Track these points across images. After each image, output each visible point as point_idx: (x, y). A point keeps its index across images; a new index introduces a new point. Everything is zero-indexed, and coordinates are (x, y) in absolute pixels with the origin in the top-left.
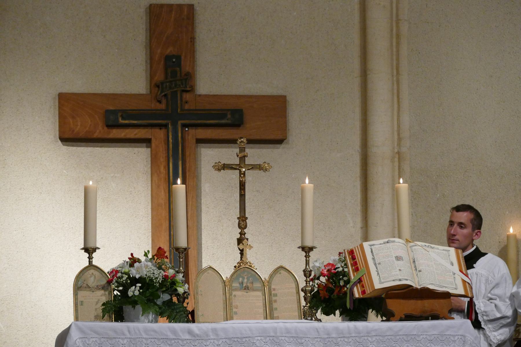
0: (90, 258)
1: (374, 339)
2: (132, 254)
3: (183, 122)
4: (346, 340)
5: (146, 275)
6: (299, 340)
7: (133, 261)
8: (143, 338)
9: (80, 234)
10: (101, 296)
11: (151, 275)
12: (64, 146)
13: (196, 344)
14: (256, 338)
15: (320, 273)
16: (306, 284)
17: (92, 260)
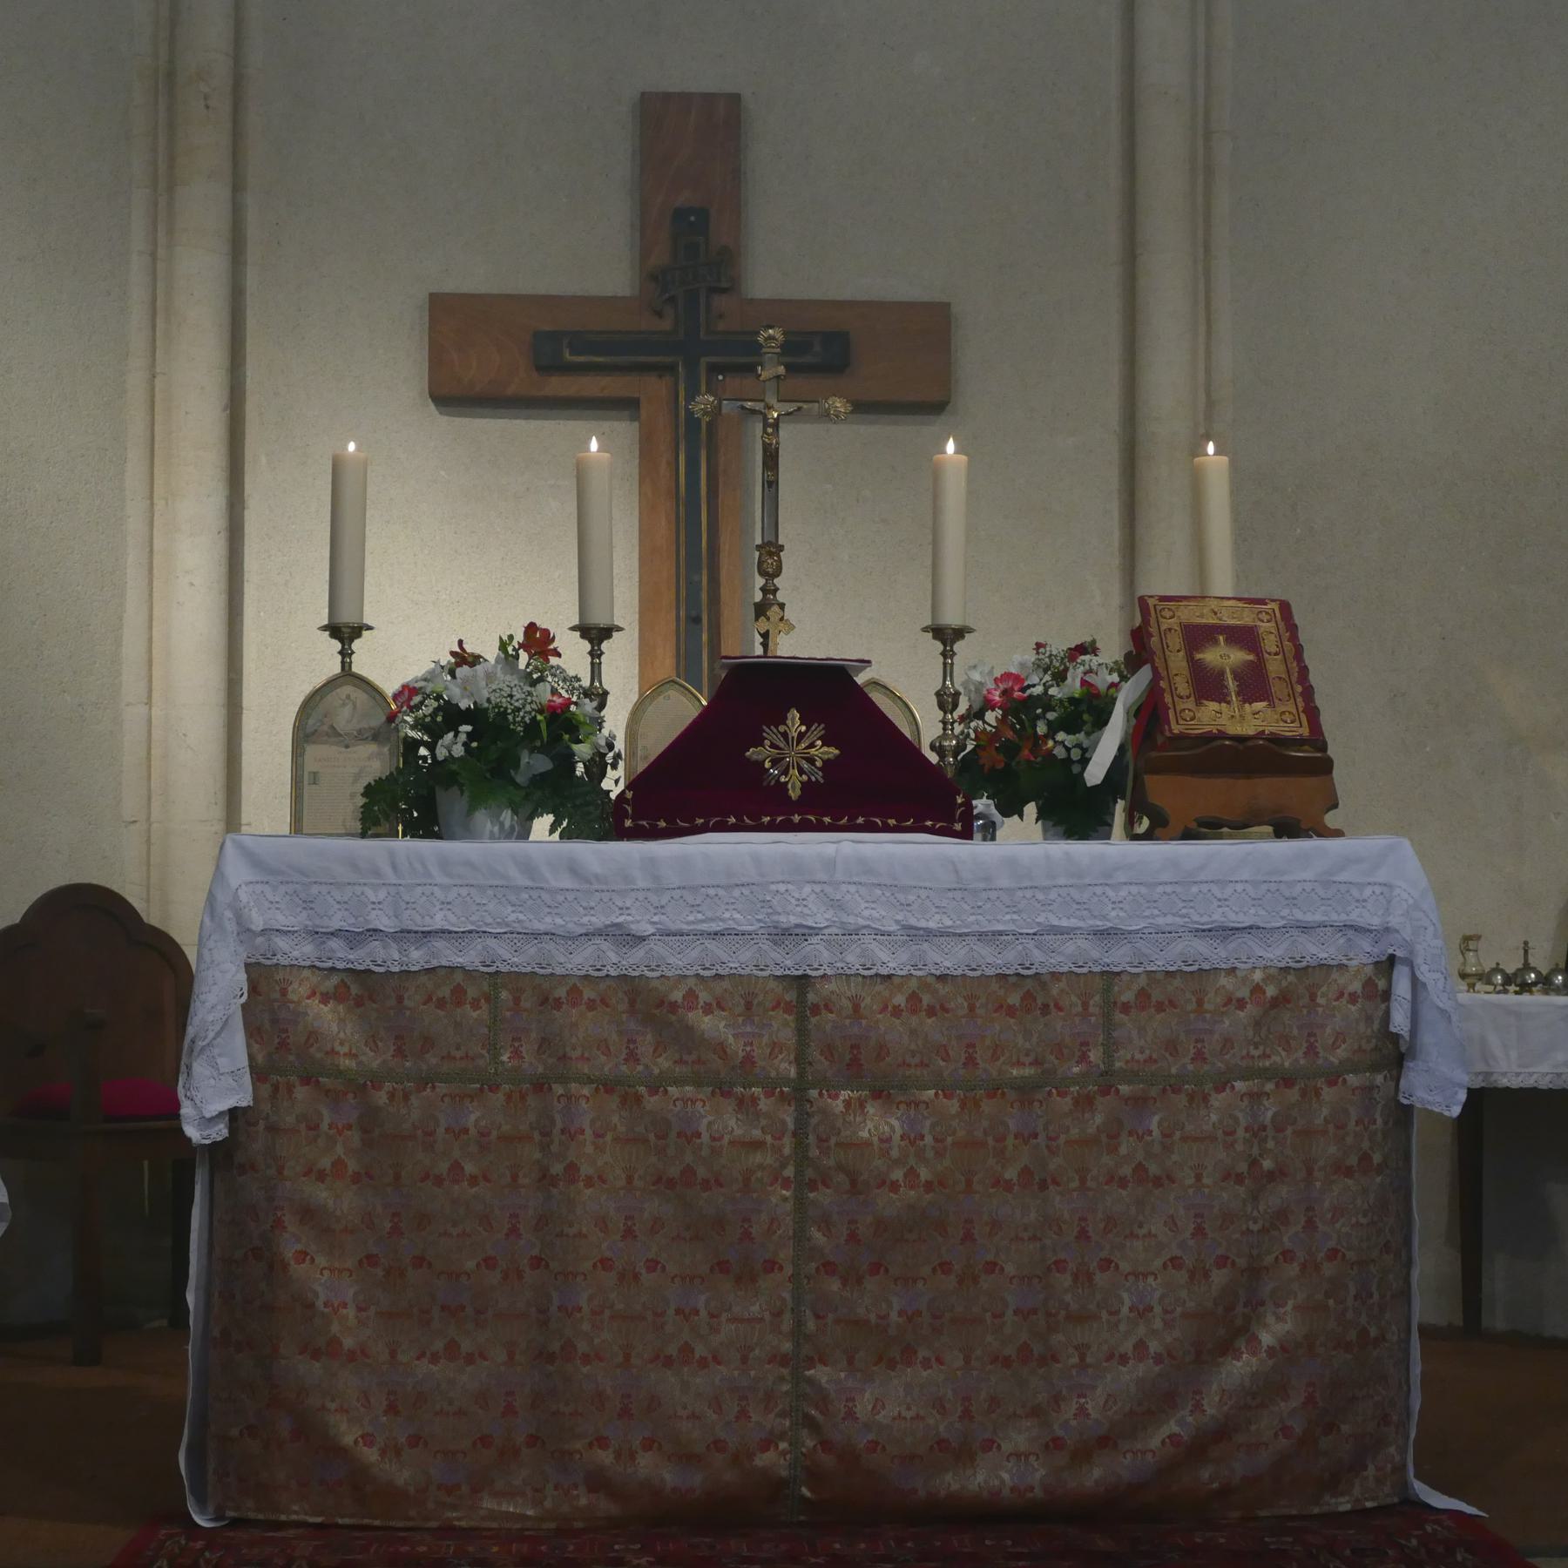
0: (346, 654)
1: (1123, 893)
2: (460, 643)
3: (714, 359)
4: (1040, 896)
5: (489, 700)
6: (901, 897)
7: (464, 658)
8: (436, 885)
9: (476, 616)
10: (369, 759)
11: (504, 700)
12: (442, 417)
13: (593, 904)
14: (773, 887)
15: (982, 699)
16: (945, 729)
17: (350, 658)
